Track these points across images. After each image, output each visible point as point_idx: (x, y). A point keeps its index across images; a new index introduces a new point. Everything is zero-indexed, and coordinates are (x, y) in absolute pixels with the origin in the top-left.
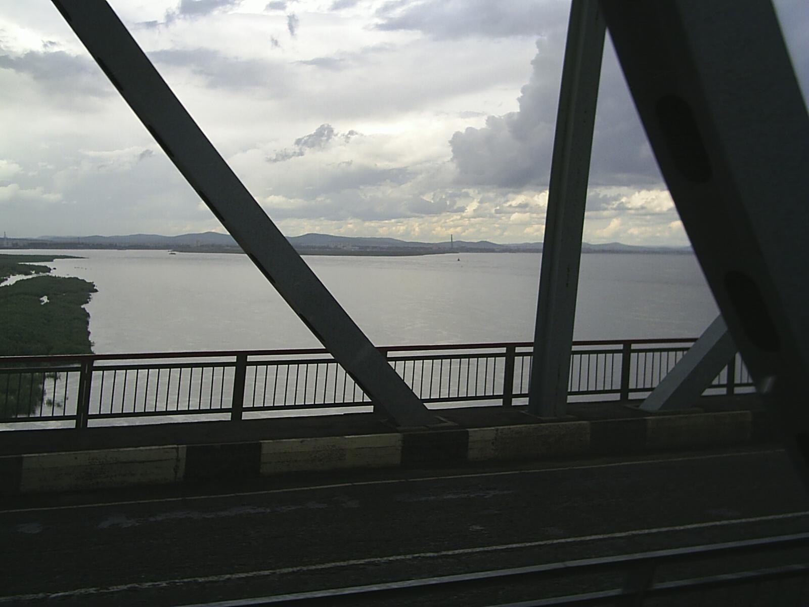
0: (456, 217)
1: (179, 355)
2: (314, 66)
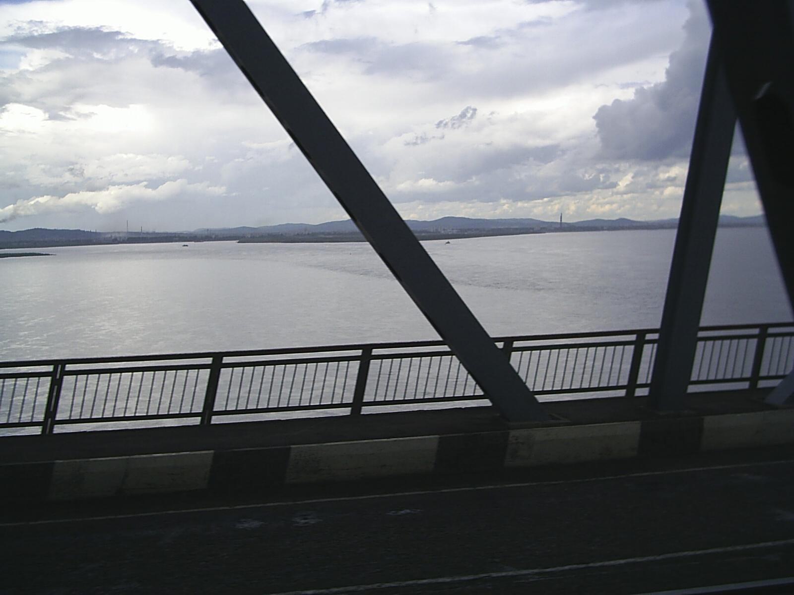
0: (610, 192)
1: (429, 344)
2: (470, 46)
